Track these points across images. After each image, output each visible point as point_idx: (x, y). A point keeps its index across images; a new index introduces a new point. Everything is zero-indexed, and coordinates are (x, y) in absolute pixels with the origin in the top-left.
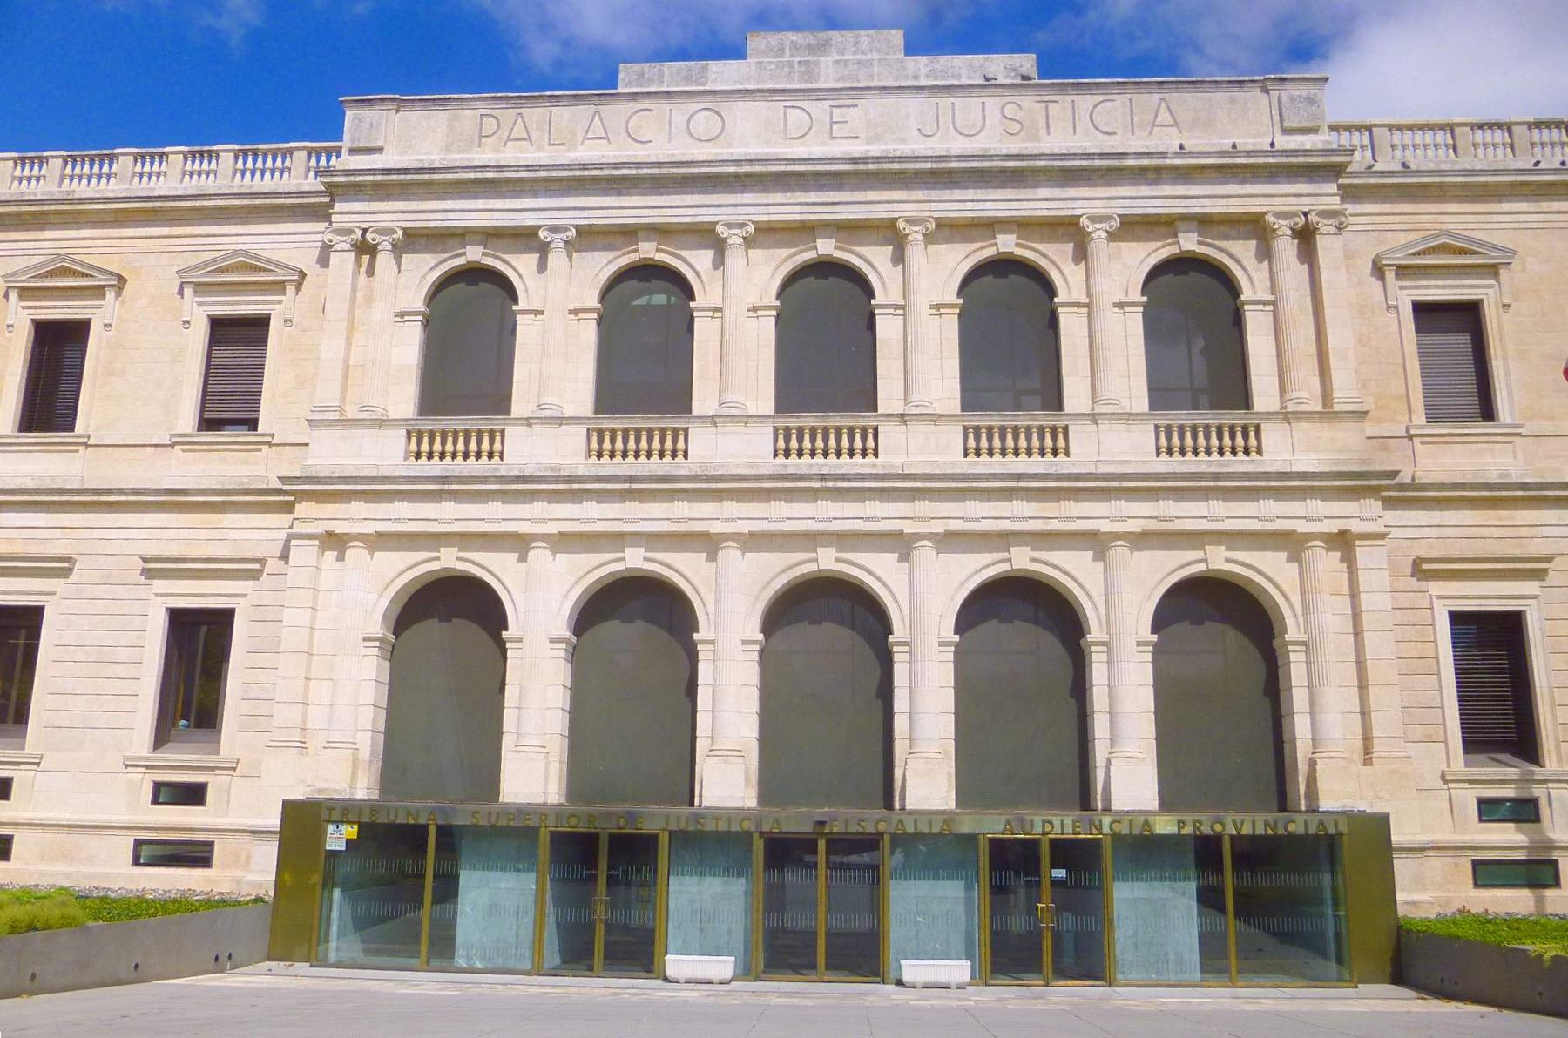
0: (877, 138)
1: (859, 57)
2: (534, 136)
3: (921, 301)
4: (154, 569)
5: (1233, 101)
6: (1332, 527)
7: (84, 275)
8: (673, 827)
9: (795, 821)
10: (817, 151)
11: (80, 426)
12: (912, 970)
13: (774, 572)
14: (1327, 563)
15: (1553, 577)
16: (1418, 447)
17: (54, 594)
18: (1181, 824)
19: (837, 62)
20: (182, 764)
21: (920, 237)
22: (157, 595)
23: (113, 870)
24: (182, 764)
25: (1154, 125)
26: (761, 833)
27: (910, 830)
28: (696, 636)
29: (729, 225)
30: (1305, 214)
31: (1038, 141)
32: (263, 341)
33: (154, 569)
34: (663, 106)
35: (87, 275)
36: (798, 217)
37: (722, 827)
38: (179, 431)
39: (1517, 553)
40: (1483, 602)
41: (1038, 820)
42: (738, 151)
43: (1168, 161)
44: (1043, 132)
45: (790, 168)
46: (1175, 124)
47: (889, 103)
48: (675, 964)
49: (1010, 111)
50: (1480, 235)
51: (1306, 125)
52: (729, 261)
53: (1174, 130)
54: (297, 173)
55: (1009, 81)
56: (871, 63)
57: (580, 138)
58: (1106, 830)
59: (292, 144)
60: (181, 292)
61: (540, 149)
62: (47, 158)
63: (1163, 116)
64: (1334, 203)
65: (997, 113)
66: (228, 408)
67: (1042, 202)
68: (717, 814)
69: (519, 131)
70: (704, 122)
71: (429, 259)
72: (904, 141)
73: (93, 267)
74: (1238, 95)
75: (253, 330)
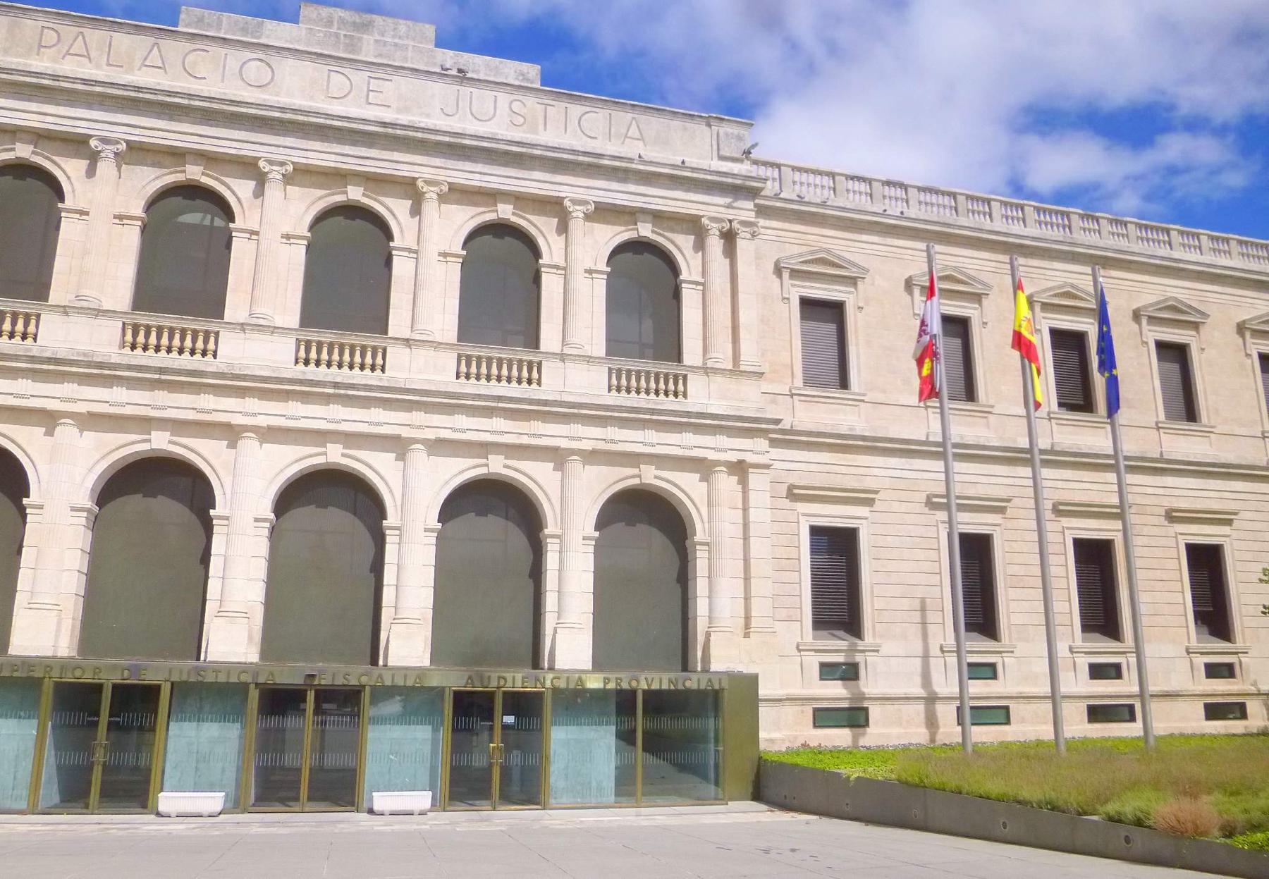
0: (406, 110)
1: (396, 41)
2: (93, 54)
3: (430, 251)
5: (685, 129)
6: (733, 457)
7: (1082, 299)
8: (175, 678)
9: (288, 674)
10: (354, 112)
12: (382, 801)
13: (289, 461)
14: (726, 483)
16: (797, 403)
18: (606, 681)
19: (376, 41)
20: (979, 649)
21: (435, 196)
25: (626, 137)
26: (257, 684)
27: (388, 683)
28: (212, 512)
29: (271, 162)
30: (730, 221)
31: (537, 134)
34: (221, 51)
37: (222, 678)
39: (856, 485)
41: (494, 676)
42: (284, 100)
44: (541, 127)
45: (329, 122)
46: (642, 139)
47: (417, 83)
48: (167, 801)
49: (516, 106)
52: (268, 192)
53: (641, 143)
55: (517, 83)
56: (405, 48)
57: (138, 63)
58: (548, 684)
61: (98, 67)
63: (634, 131)
64: (750, 216)
65: (507, 106)
67: (536, 183)
68: (218, 667)
69: (78, 47)
70: (255, 70)
72: (428, 116)
73: (850, 262)
74: (690, 125)
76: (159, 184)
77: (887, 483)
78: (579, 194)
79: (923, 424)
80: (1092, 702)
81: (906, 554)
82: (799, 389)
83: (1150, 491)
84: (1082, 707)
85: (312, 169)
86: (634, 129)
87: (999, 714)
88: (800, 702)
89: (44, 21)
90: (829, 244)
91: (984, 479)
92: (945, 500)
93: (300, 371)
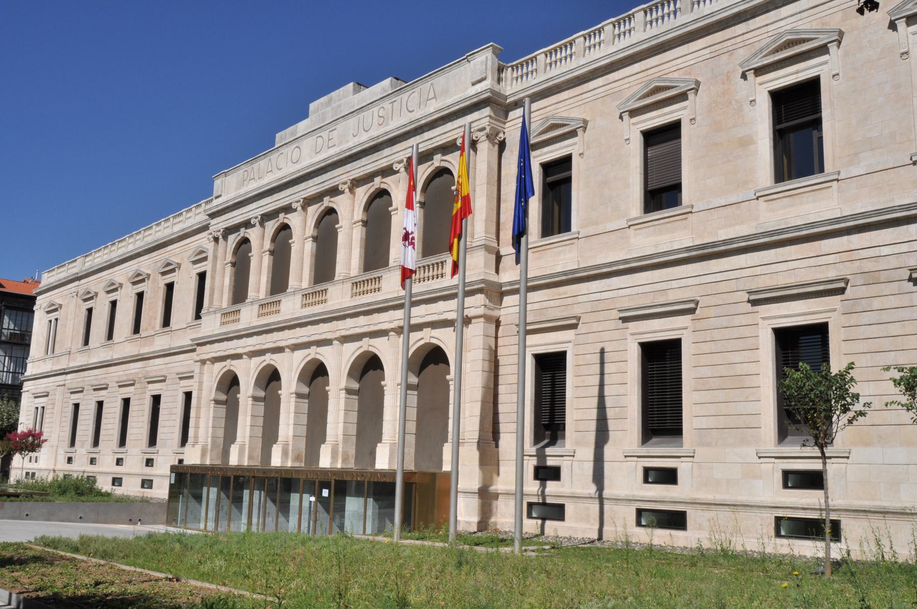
11: (574, 228)
17: (835, 310)
22: (632, 334)
23: (756, 537)
32: (679, 136)
35: (675, 87)
50: (565, 115)
54: (194, 217)
59: (633, 10)
60: (621, 117)
62: (633, 15)
66: (662, 194)
71: (315, 207)
73: (567, 119)
75: (672, 130)
76: (276, 226)
77: (701, 291)
80: (781, 513)
82: (535, 242)
83: (886, 251)
84: (769, 518)
87: (556, 512)
89: (244, 168)
90: (786, 26)
91: (675, 284)
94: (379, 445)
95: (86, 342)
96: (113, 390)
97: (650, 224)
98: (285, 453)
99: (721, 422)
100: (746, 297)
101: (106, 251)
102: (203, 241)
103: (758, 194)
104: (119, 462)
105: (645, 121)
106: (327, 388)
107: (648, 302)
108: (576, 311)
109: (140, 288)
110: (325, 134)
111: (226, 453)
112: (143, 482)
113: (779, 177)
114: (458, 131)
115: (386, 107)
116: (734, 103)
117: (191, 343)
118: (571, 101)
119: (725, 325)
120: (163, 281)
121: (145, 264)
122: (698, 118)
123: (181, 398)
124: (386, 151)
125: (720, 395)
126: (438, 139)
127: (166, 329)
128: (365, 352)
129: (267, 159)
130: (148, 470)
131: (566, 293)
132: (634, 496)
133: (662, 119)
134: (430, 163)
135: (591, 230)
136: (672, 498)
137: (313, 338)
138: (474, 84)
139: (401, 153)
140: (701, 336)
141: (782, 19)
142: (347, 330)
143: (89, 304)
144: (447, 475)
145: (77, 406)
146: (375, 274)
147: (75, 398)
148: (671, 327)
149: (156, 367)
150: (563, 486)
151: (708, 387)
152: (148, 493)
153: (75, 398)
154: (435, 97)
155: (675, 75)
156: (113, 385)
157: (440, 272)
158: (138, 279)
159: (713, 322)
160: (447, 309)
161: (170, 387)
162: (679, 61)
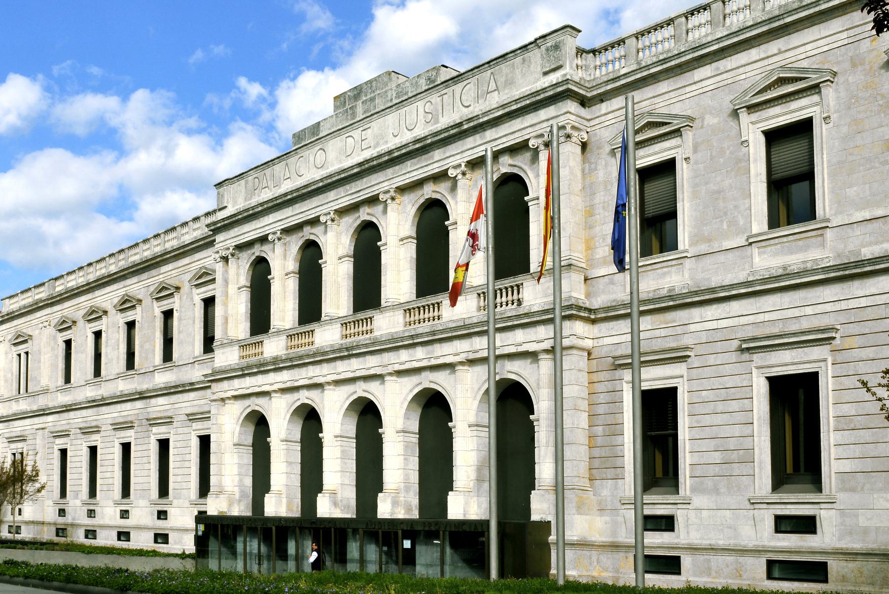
1: (369, 97)
4: (750, 347)
11: (681, 246)
15: (694, 362)
20: (796, 504)
24: (796, 504)
33: (750, 347)
35: (669, 123)
36: (348, 203)
38: (754, 231)
39: (673, 345)
40: (784, 368)
43: (481, 120)
44: (440, 115)
50: (665, 111)
51: (553, 67)
73: (670, 116)
78: (385, 186)
79: (615, 289)
81: (720, 407)
85: (515, 147)
86: (492, 84)
88: (860, 558)
91: (809, 311)
92: (630, 361)
93: (344, 341)
94: (319, 495)
95: (68, 380)
96: (108, 433)
97: (777, 241)
98: (395, 503)
99: (869, 465)
100: (735, 344)
101: (81, 274)
102: (207, 259)
103: (751, 240)
104: (125, 514)
105: (767, 119)
106: (268, 439)
107: (775, 330)
108: (687, 341)
109: (130, 316)
110: (356, 134)
111: (258, 503)
112: (156, 536)
113: (774, 223)
114: (545, 124)
115: (433, 101)
116: (879, 98)
117: (203, 378)
118: (672, 94)
119: (871, 356)
120: (158, 309)
121: (136, 286)
122: (834, 117)
123: (195, 445)
124: (437, 154)
125: (866, 435)
126: (504, 140)
127: (168, 364)
128: (425, 389)
129: (284, 163)
130: (161, 523)
131: (674, 321)
132: (763, 546)
133: (788, 117)
134: (357, 215)
135: (703, 248)
136: (811, 548)
137: (358, 374)
138: (546, 74)
139: (458, 157)
140: (695, 385)
141: (695, 83)
142: (401, 364)
143: (67, 335)
144: (545, 526)
145: (64, 452)
146: (369, 313)
147: (60, 443)
148: (806, 359)
149: (160, 406)
150: (678, 537)
151: (852, 426)
152: (162, 548)
153: (60, 443)
154: (497, 89)
155: (805, 64)
156: (106, 428)
157: (436, 314)
158: (165, 292)
159: (856, 354)
160: (538, 337)
161: (180, 430)
162: (809, 47)
